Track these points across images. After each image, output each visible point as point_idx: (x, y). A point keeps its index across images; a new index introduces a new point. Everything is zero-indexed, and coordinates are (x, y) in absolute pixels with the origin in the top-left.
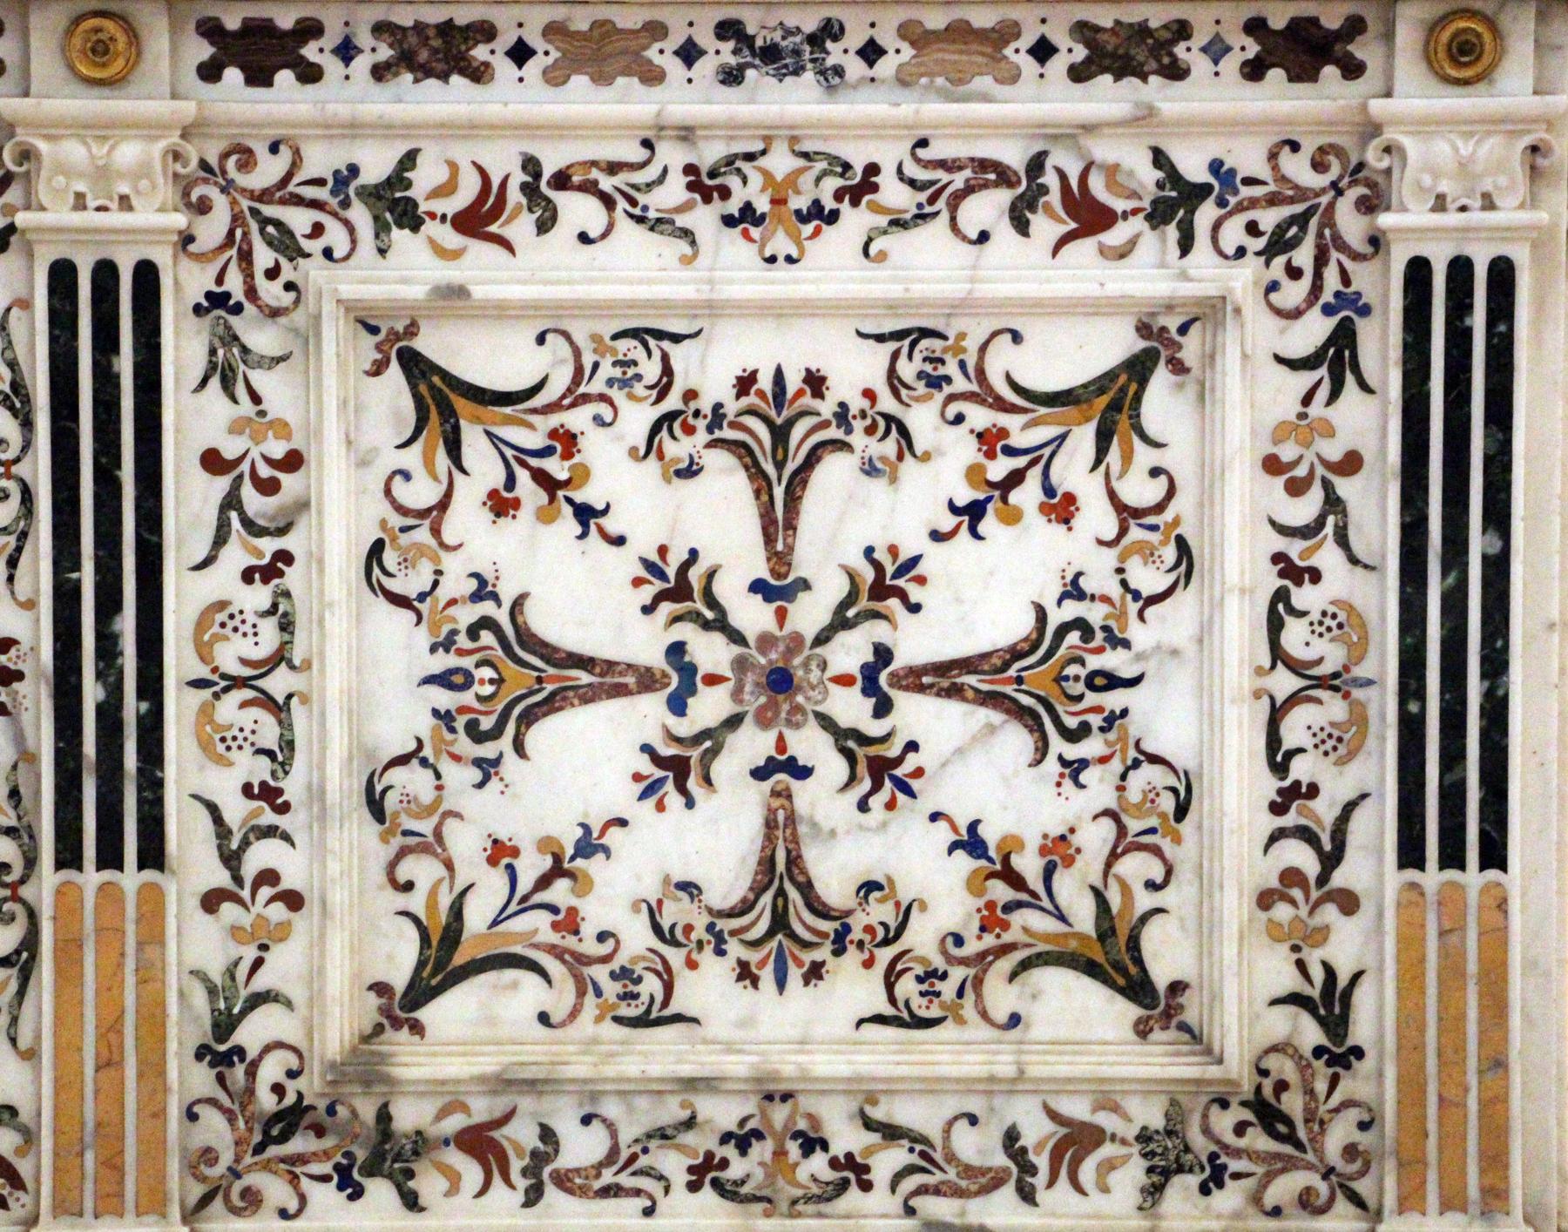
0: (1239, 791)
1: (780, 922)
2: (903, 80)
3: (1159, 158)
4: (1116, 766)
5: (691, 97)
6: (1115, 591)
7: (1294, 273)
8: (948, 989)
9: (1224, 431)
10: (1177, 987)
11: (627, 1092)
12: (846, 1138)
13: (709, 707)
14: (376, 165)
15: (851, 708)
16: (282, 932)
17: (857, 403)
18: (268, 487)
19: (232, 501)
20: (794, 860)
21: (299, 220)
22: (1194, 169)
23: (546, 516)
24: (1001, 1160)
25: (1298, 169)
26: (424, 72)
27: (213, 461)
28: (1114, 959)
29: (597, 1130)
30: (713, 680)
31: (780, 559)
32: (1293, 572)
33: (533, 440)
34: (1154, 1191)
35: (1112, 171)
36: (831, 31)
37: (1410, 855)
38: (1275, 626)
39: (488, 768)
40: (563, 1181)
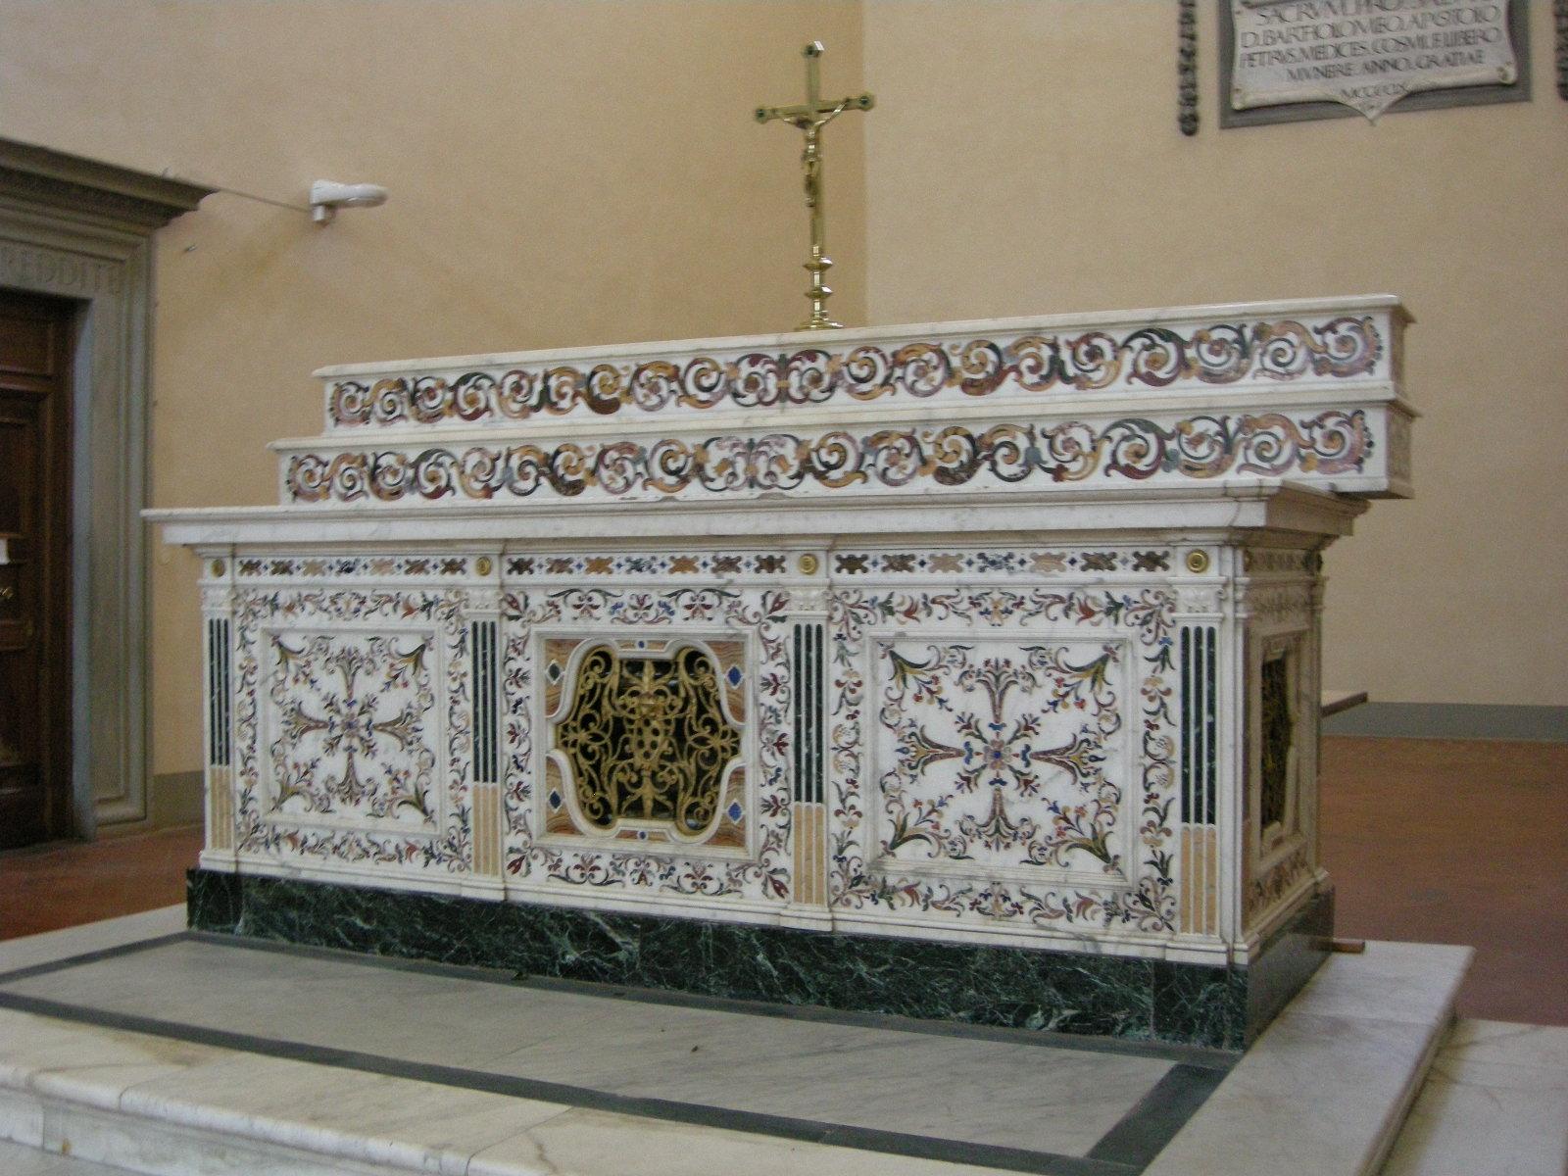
0: (1134, 795)
1: (997, 830)
2: (1032, 571)
3: (1108, 595)
4: (1098, 786)
5: (970, 575)
6: (1097, 730)
7: (1150, 631)
8: (1047, 853)
9: (1126, 681)
10: (1116, 857)
11: (953, 877)
12: (1016, 898)
13: (977, 762)
14: (882, 596)
15: (1018, 764)
16: (856, 824)
17: (1020, 669)
18: (853, 691)
19: (843, 696)
20: (1002, 811)
21: (861, 612)
22: (1119, 599)
23: (930, 702)
24: (1063, 908)
25: (1150, 599)
26: (897, 569)
27: (839, 684)
28: (1097, 847)
29: (944, 890)
30: (978, 754)
31: (997, 717)
32: (1151, 726)
33: (926, 679)
34: (1108, 921)
35: (1094, 599)
36: (1010, 556)
37: (1185, 818)
38: (1145, 742)
39: (914, 777)
40: (934, 904)
